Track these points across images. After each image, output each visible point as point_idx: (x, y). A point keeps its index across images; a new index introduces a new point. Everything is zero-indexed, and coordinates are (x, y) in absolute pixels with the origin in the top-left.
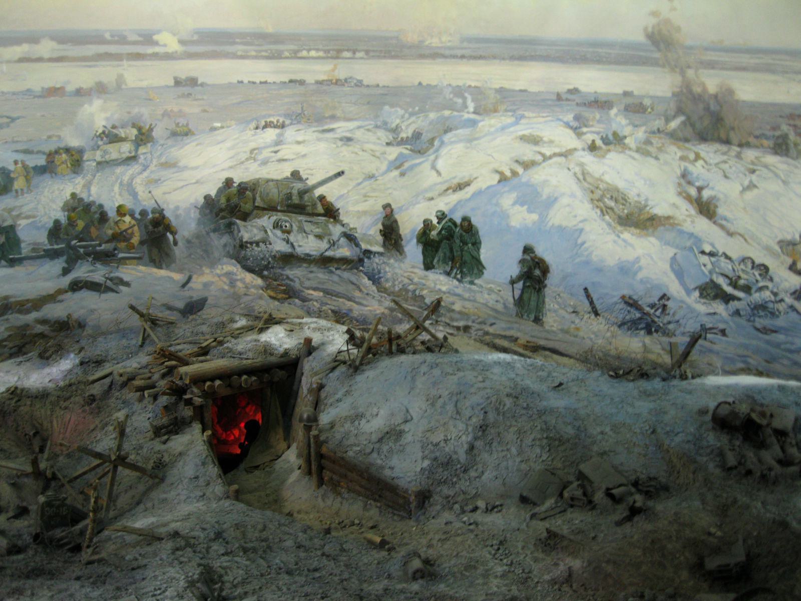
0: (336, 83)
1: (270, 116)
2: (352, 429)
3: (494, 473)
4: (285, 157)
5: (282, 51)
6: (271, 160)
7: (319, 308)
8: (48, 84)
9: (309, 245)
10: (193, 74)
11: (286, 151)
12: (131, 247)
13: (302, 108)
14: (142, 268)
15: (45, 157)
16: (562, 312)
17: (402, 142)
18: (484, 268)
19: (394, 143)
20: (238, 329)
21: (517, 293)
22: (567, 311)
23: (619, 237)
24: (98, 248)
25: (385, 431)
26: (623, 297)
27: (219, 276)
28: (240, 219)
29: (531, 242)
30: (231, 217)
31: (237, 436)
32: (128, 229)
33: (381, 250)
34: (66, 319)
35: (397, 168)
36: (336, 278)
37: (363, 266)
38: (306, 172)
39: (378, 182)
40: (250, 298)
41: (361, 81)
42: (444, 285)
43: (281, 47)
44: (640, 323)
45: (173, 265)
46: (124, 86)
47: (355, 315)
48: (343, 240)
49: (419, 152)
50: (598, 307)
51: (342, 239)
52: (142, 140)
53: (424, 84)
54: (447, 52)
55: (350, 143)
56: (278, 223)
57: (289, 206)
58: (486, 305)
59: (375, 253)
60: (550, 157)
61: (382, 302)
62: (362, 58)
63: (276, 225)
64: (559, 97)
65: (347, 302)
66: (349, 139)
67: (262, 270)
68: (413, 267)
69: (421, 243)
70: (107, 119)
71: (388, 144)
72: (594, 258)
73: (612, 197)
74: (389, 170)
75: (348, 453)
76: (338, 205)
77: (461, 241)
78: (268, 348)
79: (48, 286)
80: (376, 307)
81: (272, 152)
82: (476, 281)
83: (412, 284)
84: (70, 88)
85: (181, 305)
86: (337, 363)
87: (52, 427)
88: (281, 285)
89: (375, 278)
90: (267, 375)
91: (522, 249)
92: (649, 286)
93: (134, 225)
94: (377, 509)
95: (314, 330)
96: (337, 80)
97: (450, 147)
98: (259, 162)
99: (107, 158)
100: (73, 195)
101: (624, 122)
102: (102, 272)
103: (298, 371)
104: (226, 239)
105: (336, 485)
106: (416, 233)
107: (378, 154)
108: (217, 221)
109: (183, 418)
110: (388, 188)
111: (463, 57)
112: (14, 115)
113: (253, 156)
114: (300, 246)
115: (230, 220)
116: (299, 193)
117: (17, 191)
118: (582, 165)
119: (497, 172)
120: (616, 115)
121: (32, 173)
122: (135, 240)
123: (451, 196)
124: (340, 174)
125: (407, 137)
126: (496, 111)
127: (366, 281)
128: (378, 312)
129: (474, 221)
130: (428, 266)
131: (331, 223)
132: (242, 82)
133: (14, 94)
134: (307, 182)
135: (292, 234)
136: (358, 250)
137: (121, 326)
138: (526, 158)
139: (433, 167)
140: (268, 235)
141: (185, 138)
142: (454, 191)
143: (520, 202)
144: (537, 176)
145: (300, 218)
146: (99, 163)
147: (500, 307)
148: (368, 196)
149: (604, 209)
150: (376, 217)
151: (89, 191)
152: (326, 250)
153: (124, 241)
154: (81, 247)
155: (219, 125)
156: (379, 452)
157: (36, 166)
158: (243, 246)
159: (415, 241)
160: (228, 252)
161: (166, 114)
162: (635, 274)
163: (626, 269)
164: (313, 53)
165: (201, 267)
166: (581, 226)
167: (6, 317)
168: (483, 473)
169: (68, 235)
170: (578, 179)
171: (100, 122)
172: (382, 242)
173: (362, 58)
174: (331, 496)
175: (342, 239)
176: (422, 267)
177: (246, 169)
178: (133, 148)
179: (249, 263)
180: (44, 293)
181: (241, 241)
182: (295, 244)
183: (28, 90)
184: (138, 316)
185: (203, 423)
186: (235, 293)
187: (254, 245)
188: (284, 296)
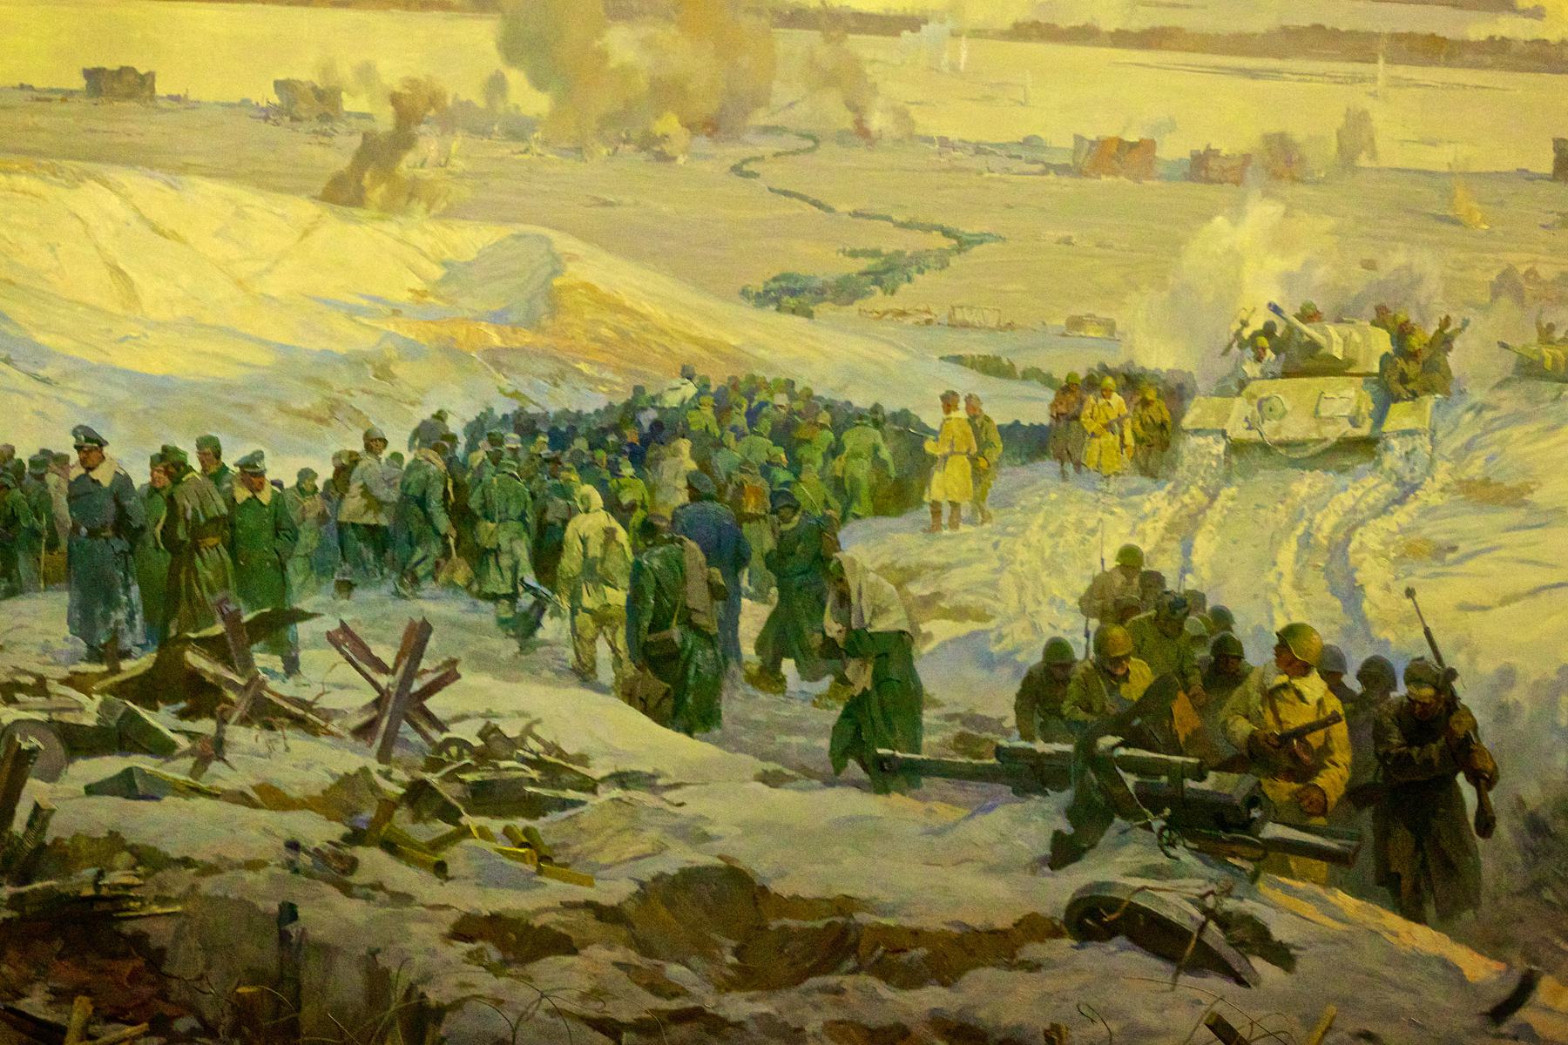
8: (1106, 128)
12: (1306, 809)
14: (1344, 900)
15: (1050, 395)
24: (1190, 784)
32: (1311, 728)
46: (1363, 161)
52: (1404, 379)
84: (1173, 149)
93: (1335, 718)
100: (1130, 558)
102: (1195, 886)
112: (970, 228)
117: (936, 508)
122: (1333, 780)
133: (979, 149)
146: (1236, 448)
151: (1187, 551)
153: (1290, 775)
154: (1131, 765)
161: (1507, 285)
167: (832, 980)
169: (1089, 709)
178: (1368, 406)
180: (977, 922)
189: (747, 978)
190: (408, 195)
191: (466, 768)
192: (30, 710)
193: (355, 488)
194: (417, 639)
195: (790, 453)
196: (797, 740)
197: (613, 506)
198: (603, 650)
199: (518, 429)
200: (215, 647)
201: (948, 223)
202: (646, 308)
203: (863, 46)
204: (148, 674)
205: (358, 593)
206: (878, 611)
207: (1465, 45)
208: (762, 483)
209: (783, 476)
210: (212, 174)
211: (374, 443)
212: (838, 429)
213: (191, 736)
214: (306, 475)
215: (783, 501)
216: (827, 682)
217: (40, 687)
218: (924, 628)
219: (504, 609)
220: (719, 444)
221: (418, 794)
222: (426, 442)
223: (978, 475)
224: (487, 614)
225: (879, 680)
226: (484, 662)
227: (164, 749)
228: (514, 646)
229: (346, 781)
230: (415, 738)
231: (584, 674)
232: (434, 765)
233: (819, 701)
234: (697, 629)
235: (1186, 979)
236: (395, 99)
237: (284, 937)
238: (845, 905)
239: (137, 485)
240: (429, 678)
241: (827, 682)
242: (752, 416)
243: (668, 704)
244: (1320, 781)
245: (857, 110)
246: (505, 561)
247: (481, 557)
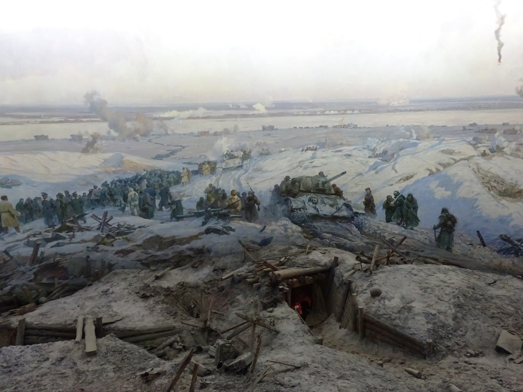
0: (343, 127)
1: (309, 144)
2: (380, 305)
3: (473, 333)
4: (316, 165)
5: (317, 112)
8: (202, 130)
9: (326, 210)
10: (272, 124)
11: (316, 162)
12: (236, 212)
13: (326, 140)
14: (241, 222)
15: (198, 166)
16: (464, 245)
17: (377, 156)
18: (419, 221)
19: (373, 157)
21: (438, 234)
22: (466, 244)
23: (499, 202)
24: (221, 212)
26: (501, 236)
27: (280, 226)
28: (292, 197)
29: (446, 206)
32: (236, 202)
33: (364, 212)
34: (202, 248)
35: (374, 169)
36: (339, 227)
37: (353, 221)
39: (363, 177)
40: (294, 237)
41: (356, 125)
42: (397, 230)
43: (315, 109)
44: (512, 250)
45: (257, 221)
46: (237, 131)
49: (386, 161)
50: (485, 241)
52: (245, 158)
53: (390, 125)
54: (402, 109)
55: (349, 157)
57: (317, 190)
58: (419, 241)
60: (459, 161)
62: (357, 114)
63: (310, 200)
64: (464, 128)
65: (344, 239)
66: (349, 155)
68: (380, 221)
70: (229, 147)
71: (369, 157)
72: (484, 214)
73: (495, 181)
74: (370, 170)
76: (342, 189)
77: (407, 207)
79: (195, 231)
81: (310, 163)
82: (415, 228)
83: (380, 230)
84: (212, 132)
85: (259, 241)
87: (202, 303)
89: (359, 227)
91: (441, 210)
92: (518, 229)
93: (239, 200)
96: (344, 125)
97: (402, 158)
98: (303, 168)
99: (228, 166)
100: (210, 185)
101: (503, 139)
102: (222, 224)
104: (284, 207)
107: (364, 162)
110: (369, 180)
111: (410, 110)
112: (184, 145)
114: (321, 210)
116: (322, 183)
117: (183, 183)
118: (477, 164)
119: (428, 170)
120: (498, 136)
121: (191, 174)
122: (239, 208)
123: (403, 183)
124: (344, 173)
125: (380, 153)
126: (428, 138)
127: (355, 229)
128: (360, 245)
129: (415, 196)
130: (388, 220)
131: (338, 198)
132: (296, 128)
133: (184, 134)
135: (318, 204)
136: (351, 212)
137: (233, 251)
138: (444, 162)
139: (393, 168)
141: (267, 156)
142: (404, 181)
143: (441, 185)
144: (451, 171)
146: (224, 169)
147: (427, 242)
149: (490, 187)
151: (218, 183)
152: (335, 213)
153: (234, 208)
154: (212, 211)
155: (284, 149)
157: (193, 170)
158: (292, 210)
159: (382, 207)
160: (285, 214)
161: (258, 144)
162: (509, 222)
163: (502, 220)
164: (332, 112)
165: (271, 221)
166: (476, 197)
167: (172, 247)
168: (466, 332)
169: (206, 205)
170: (475, 172)
171: (225, 149)
173: (357, 114)
176: (385, 221)
177: (296, 171)
178: (241, 161)
179: (295, 220)
180: (192, 235)
183: (192, 133)
184: (241, 246)
188: (312, 236)
189: (160, 249)
190: (96, 150)
191: (115, 231)
192: (39, 237)
193: (93, 194)
194: (106, 214)
195: (161, 179)
196: (165, 217)
197: (135, 190)
198: (135, 210)
199: (119, 182)
200: (72, 222)
201: (182, 145)
202: (137, 162)
203: (166, 122)
204: (60, 228)
205: (95, 209)
206: (176, 198)
207: (250, 115)
208: (157, 184)
209: (160, 182)
210: (62, 150)
211: (95, 187)
212: (168, 175)
213: (68, 235)
214: (84, 194)
215: (161, 185)
216: (169, 208)
217: (40, 233)
218: (183, 199)
219: (119, 207)
220: (150, 179)
221: (108, 236)
222: (104, 186)
223: (189, 178)
224: (117, 208)
225: (177, 207)
226: (117, 215)
227: (64, 238)
228: (122, 212)
229: (96, 236)
230: (107, 228)
231: (133, 214)
232: (110, 231)
233: (168, 211)
234: (149, 205)
235: (221, 236)
236: (92, 136)
237: (87, 261)
238: (174, 237)
239: (54, 200)
240: (108, 219)
241: (169, 208)
242: (155, 175)
243: (146, 216)
244: (238, 208)
245: (166, 131)
246: (119, 201)
247: (115, 201)
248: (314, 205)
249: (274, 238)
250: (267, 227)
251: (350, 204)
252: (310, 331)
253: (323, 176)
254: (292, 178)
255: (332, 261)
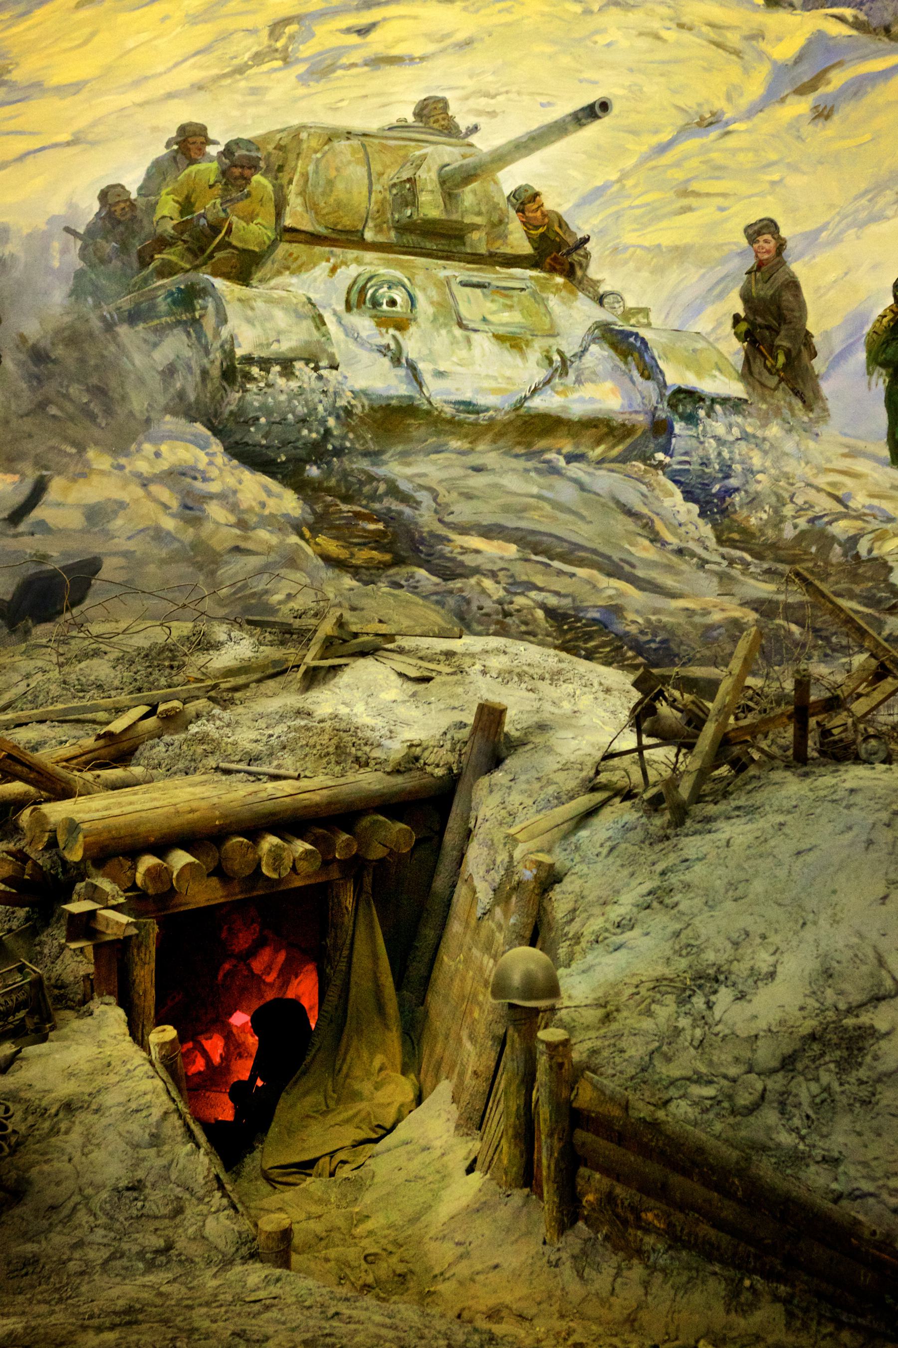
2: (684, 1022)
4: (395, 52)
6: (345, 61)
7: (500, 602)
20: (230, 673)
25: (805, 1030)
27: (145, 483)
28: (227, 276)
30: (196, 268)
31: (217, 1060)
33: (736, 389)
35: (802, 91)
37: (667, 451)
38: (473, 103)
39: (731, 142)
40: (253, 562)
47: (633, 629)
48: (598, 352)
49: (887, 30)
51: (594, 348)
56: (363, 290)
57: (403, 228)
59: (713, 401)
61: (731, 578)
65: (603, 581)
67: (300, 462)
68: (853, 453)
69: (884, 365)
75: (672, 1107)
78: (346, 737)
80: (711, 599)
81: (348, 31)
86: (599, 796)
88: (369, 518)
90: (345, 836)
94: (779, 1307)
95: (505, 676)
98: (301, 68)
103: (454, 823)
105: (625, 1223)
106: (868, 329)
107: (733, 39)
108: (146, 280)
109: (61, 985)
113: (279, 45)
114: (440, 374)
115: (192, 276)
116: (443, 183)
128: (716, 617)
131: (558, 289)
134: (473, 139)
135: (413, 329)
136: (650, 388)
140: (326, 335)
145: (443, 274)
148: (696, 194)
150: (721, 271)
152: (535, 391)
156: (783, 1104)
159: (862, 356)
160: (181, 395)
165: (81, 448)
172: (738, 360)
174: (610, 1262)
175: (594, 348)
176: (885, 453)
179: (255, 435)
181: (229, 354)
182: (421, 366)
185: (126, 1002)
186: (198, 546)
187: (277, 369)
248: (387, 337)
249: (110, 569)
250: (56, 488)
251: (643, 332)
252: (221, 1187)
253: (450, 130)
254: (223, 142)
255: (465, 733)
